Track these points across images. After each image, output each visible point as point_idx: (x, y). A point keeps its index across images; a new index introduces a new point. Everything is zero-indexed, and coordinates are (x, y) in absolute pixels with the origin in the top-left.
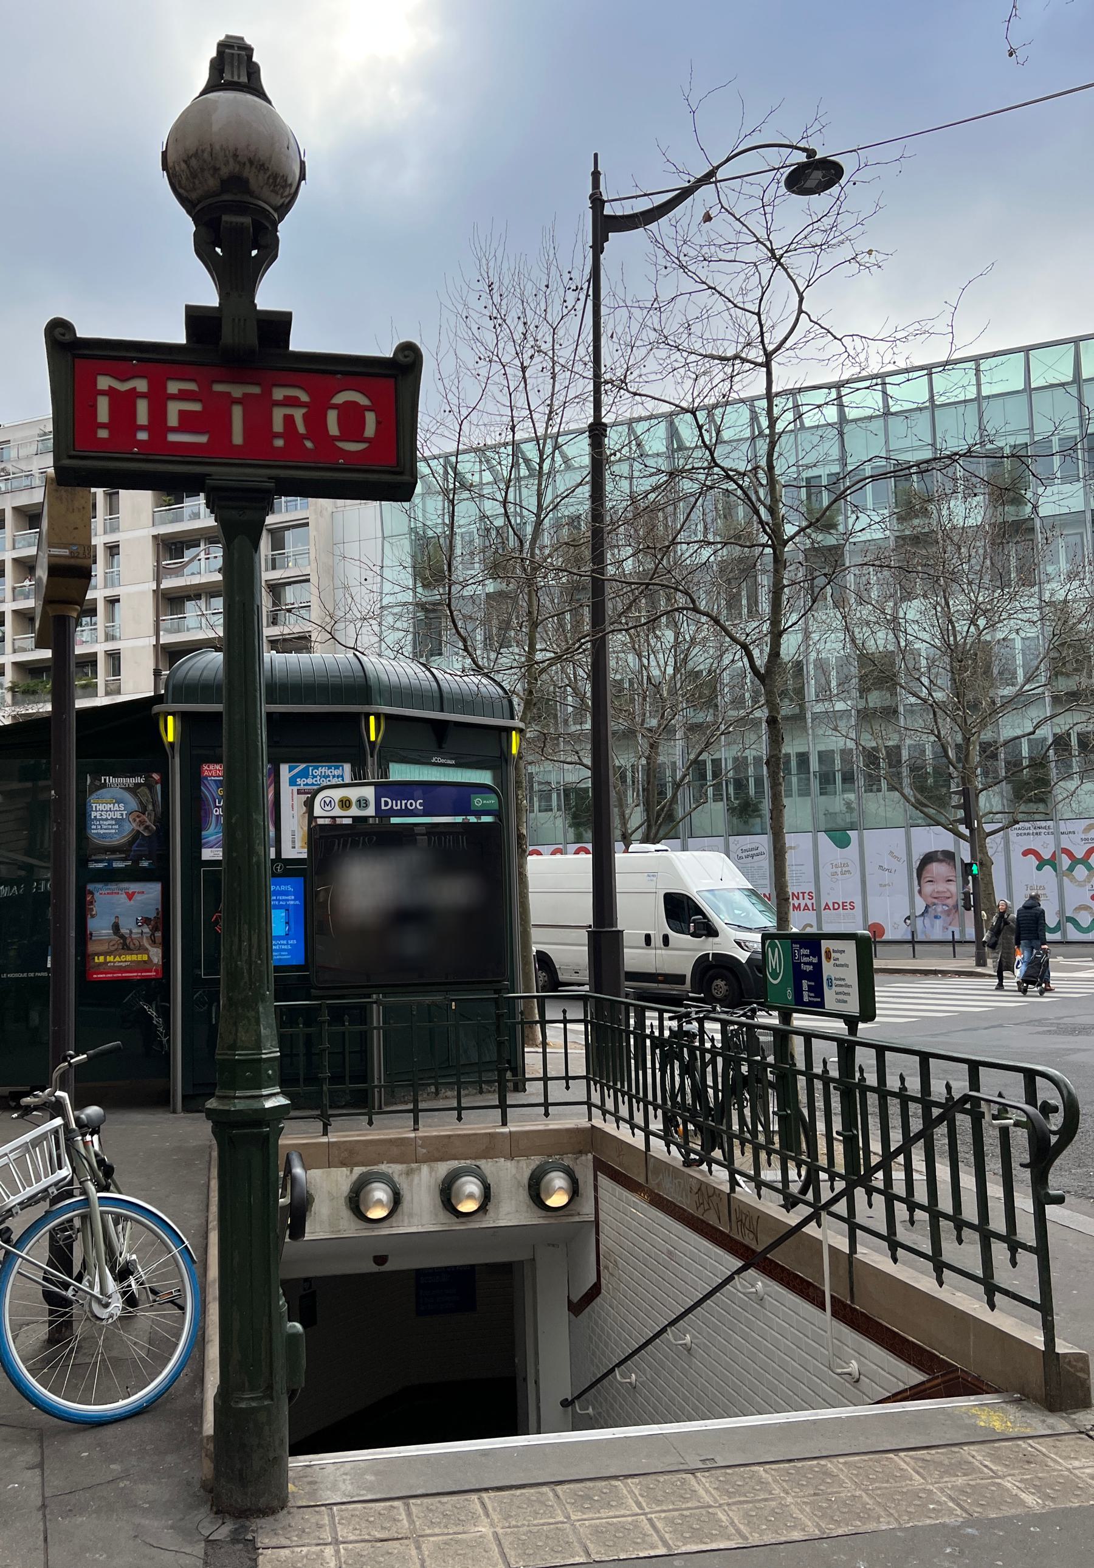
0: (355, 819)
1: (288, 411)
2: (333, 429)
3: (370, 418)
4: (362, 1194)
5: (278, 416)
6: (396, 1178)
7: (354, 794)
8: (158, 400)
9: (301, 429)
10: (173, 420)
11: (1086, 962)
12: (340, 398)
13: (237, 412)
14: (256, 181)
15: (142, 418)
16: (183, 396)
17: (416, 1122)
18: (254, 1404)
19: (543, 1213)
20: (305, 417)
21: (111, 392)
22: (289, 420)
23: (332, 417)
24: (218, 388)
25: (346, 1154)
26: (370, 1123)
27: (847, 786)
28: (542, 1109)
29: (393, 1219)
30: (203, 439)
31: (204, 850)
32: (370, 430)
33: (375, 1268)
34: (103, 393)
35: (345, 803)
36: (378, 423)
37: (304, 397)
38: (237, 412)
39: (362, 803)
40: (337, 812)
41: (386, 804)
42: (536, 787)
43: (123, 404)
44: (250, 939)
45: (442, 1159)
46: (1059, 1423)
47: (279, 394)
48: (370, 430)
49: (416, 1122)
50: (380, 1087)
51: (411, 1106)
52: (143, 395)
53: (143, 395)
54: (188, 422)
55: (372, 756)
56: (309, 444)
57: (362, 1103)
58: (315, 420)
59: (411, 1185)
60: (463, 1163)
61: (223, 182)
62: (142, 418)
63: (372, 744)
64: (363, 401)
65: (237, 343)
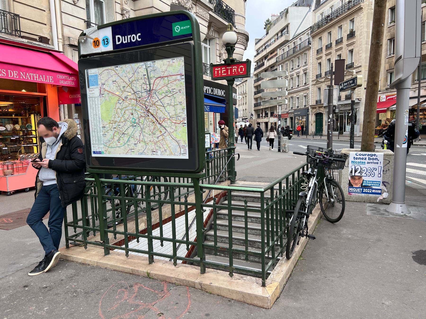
2: (239, 71)
3: (243, 69)
5: (233, 70)
8: (221, 70)
11: (423, 150)
16: (224, 69)
23: (239, 69)
27: (50, 42)
31: (213, 113)
32: (243, 70)
37: (236, 67)
42: (326, 138)
43: (218, 71)
47: (233, 67)
48: (243, 70)
54: (224, 72)
58: (237, 70)
64: (243, 67)
65: (230, 62)
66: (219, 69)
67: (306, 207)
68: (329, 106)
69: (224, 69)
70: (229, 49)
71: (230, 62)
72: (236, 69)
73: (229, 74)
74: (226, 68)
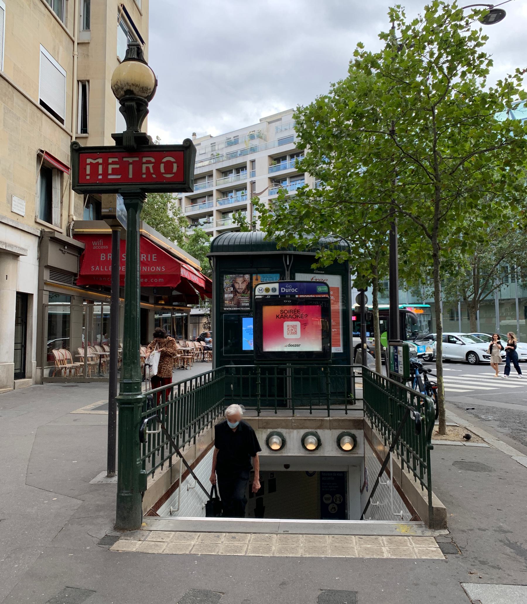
0: (271, 296)
1: (148, 164)
2: (162, 170)
3: (175, 165)
4: (306, 439)
5: (144, 166)
6: (284, 434)
7: (270, 286)
8: (106, 165)
9: (152, 171)
10: (110, 171)
12: (165, 160)
13: (131, 167)
14: (136, 90)
15: (100, 172)
16: (114, 163)
17: (293, 413)
18: (126, 495)
19: (343, 452)
20: (153, 166)
21: (91, 164)
22: (148, 168)
23: (162, 166)
24: (125, 159)
25: (265, 424)
26: (276, 413)
28: (309, 411)
29: (354, 450)
30: (119, 177)
32: (175, 170)
33: (285, 470)
34: (88, 164)
35: (267, 290)
36: (178, 167)
37: (153, 160)
38: (131, 167)
39: (274, 290)
40: (265, 293)
41: (283, 290)
43: (95, 167)
44: (129, 343)
45: (302, 428)
46: (429, 533)
47: (144, 160)
48: (175, 170)
49: (293, 413)
50: (290, 399)
51: (309, 407)
52: (101, 164)
53: (101, 164)
55: (288, 271)
56: (154, 176)
57: (282, 405)
58: (156, 168)
59: (290, 436)
60: (310, 430)
61: (125, 92)
62: (100, 172)
63: (288, 266)
64: (172, 159)
65: (134, 143)
66: (100, 161)
67: (316, 242)
68: (391, 204)
69: (114, 163)
70: (131, 107)
71: (133, 143)
72: (151, 166)
73: (131, 176)
74: (121, 159)
